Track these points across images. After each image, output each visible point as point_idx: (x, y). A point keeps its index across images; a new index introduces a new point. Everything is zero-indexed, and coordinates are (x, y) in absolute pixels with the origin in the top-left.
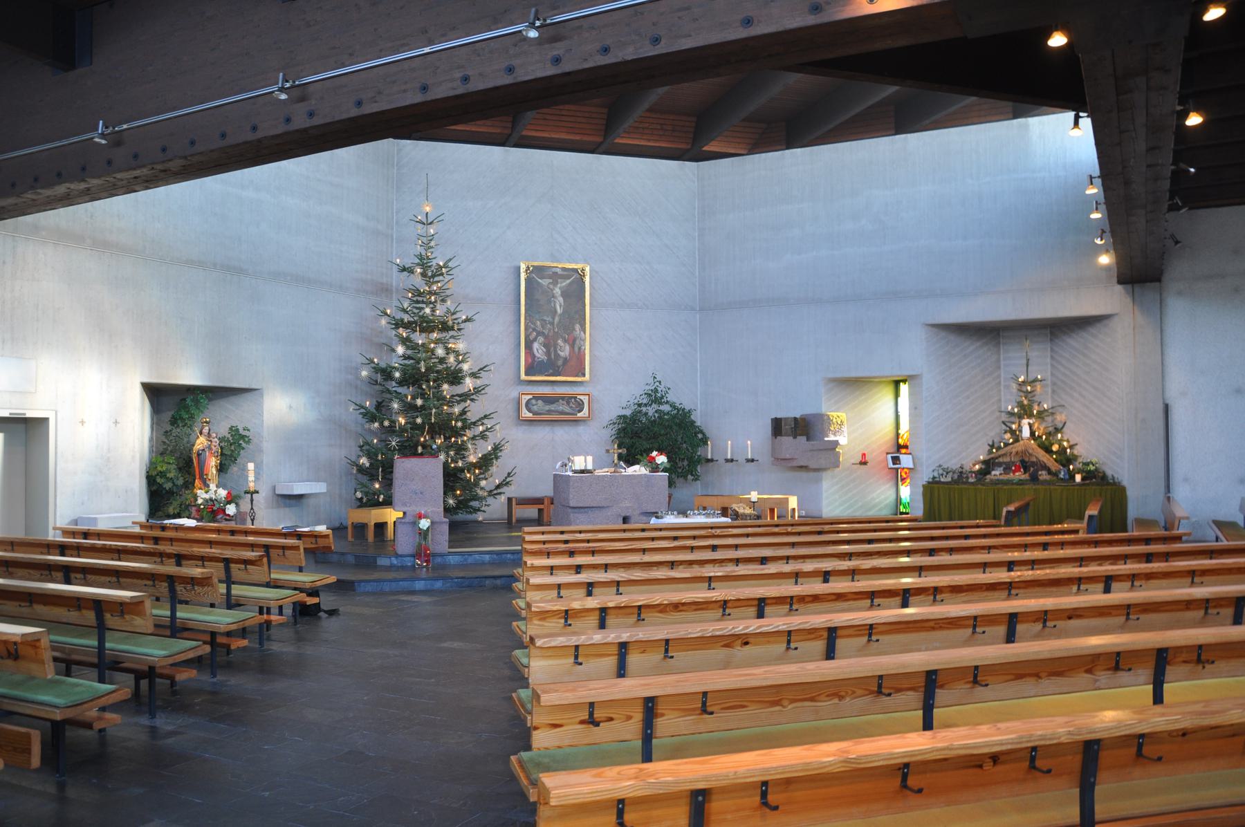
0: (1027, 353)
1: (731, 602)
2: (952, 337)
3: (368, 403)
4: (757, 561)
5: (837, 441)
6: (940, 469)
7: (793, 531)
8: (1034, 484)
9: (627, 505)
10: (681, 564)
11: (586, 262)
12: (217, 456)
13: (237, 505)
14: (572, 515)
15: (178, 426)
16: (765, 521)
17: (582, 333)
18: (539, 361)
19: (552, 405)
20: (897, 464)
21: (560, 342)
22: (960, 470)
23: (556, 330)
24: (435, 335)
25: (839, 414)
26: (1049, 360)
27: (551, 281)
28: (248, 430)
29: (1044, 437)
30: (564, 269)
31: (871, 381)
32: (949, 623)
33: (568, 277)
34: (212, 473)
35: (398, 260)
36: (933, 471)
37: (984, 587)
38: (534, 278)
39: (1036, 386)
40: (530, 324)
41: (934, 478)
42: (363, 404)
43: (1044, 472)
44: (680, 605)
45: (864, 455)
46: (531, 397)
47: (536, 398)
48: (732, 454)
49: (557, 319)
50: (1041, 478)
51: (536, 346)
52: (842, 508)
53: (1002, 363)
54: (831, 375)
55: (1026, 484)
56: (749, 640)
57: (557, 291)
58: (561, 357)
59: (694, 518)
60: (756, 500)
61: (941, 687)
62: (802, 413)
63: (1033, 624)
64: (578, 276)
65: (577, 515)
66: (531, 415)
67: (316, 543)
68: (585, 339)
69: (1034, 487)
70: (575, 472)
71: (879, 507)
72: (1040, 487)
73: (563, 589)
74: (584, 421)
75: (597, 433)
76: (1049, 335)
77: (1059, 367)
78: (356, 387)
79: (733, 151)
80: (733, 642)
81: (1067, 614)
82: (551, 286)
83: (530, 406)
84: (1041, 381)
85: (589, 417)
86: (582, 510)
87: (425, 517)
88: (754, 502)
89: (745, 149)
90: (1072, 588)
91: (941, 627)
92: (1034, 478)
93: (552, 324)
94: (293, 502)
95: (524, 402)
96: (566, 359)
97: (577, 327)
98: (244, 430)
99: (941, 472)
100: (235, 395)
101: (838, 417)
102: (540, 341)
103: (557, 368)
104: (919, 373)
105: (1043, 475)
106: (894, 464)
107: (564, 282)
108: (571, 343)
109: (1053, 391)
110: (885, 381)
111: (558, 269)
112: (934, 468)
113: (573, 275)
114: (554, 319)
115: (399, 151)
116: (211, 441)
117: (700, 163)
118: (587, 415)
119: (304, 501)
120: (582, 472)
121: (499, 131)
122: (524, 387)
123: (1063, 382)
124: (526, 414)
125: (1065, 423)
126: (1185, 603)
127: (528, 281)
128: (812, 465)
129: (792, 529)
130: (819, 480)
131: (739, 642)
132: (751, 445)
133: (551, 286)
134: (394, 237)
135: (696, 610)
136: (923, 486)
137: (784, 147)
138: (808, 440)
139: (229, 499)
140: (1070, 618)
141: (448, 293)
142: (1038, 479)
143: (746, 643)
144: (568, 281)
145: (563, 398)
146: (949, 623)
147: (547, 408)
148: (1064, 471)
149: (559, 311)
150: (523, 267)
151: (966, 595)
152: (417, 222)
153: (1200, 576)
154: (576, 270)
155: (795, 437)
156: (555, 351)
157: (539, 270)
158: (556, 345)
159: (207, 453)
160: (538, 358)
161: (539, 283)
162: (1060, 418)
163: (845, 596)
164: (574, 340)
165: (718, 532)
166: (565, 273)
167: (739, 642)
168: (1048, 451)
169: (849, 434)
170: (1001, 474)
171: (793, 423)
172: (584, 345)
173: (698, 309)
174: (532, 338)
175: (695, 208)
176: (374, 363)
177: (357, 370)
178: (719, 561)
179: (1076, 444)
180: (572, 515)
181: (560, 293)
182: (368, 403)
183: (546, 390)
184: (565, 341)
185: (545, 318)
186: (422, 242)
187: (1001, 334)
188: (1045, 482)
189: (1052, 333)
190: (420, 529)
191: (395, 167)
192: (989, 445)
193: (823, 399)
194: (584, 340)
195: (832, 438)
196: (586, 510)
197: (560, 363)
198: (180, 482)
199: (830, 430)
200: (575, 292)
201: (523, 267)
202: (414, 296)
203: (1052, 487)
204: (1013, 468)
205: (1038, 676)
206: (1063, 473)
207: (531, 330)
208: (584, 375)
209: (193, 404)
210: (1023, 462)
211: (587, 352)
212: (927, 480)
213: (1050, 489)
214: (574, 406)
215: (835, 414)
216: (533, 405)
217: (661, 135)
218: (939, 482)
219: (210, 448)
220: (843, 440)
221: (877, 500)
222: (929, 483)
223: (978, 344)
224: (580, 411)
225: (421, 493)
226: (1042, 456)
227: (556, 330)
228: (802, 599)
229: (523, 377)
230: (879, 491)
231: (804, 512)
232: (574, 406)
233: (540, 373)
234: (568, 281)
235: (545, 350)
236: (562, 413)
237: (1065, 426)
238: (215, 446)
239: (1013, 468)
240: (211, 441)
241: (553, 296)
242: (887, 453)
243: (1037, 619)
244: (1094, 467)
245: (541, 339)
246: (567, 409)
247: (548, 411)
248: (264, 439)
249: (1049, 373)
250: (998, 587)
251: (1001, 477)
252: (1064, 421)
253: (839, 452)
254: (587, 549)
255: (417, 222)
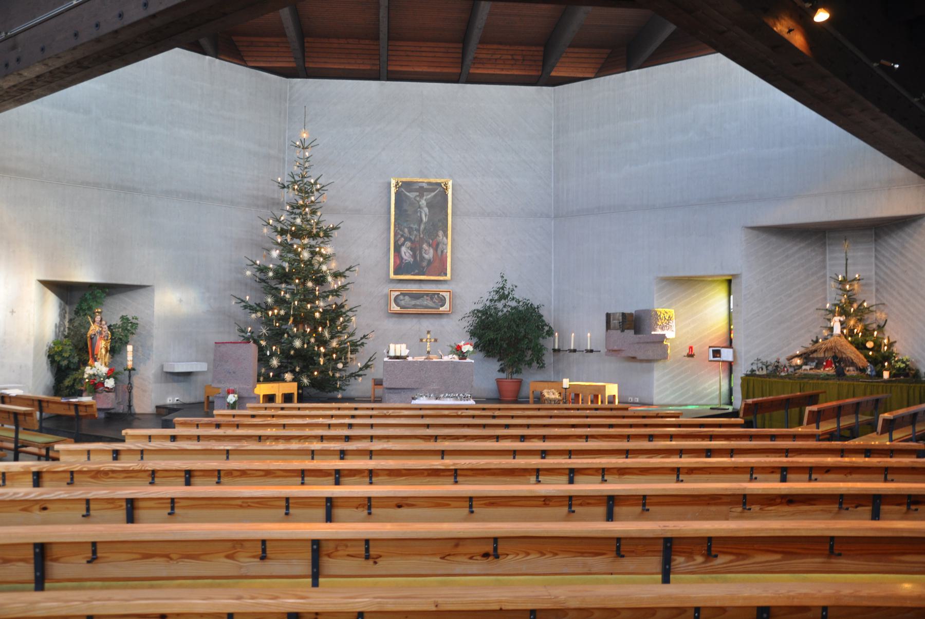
0: (846, 253)
1: (160, 472)
2: (773, 239)
3: (248, 297)
4: (341, 439)
5: (664, 335)
6: (759, 362)
7: (463, 414)
8: (839, 380)
9: (435, 387)
10: (268, 439)
11: (451, 177)
12: (107, 340)
13: (116, 379)
14: (387, 395)
15: (80, 315)
16: (577, 405)
17: (445, 238)
18: (406, 263)
19: (418, 301)
20: (717, 357)
21: (425, 246)
22: (776, 364)
23: (422, 236)
24: (306, 241)
25: (667, 310)
26: (873, 259)
27: (418, 194)
28: (136, 319)
29: (860, 334)
30: (429, 184)
31: (704, 281)
32: (258, 503)
33: (433, 190)
34: (101, 354)
35: (279, 179)
36: (752, 364)
37: (426, 473)
38: (402, 191)
39: (853, 285)
40: (398, 231)
41: (753, 371)
42: (244, 299)
43: (851, 368)
44: (110, 473)
45: (691, 348)
46: (398, 293)
47: (404, 294)
48: (559, 346)
49: (422, 227)
50: (848, 374)
51: (403, 249)
52: (672, 397)
53: (828, 262)
54: (662, 275)
55: (831, 379)
56: (47, 505)
57: (423, 202)
58: (425, 259)
59: (444, 400)
60: (568, 387)
61: (56, 560)
62: (637, 309)
63: (355, 510)
64: (442, 189)
65: (391, 395)
66: (398, 308)
67: (86, 412)
68: (447, 244)
69: (838, 383)
70: (391, 358)
71: (711, 397)
72: (844, 382)
73: (232, 454)
74: (448, 314)
75: (458, 325)
76: (874, 236)
77: (881, 266)
78: (246, 285)
79: (581, 75)
80: (31, 506)
81: (396, 503)
82: (418, 199)
83: (399, 301)
84: (859, 280)
85: (450, 311)
86: (397, 391)
87: (233, 392)
88: (566, 389)
89: (592, 72)
90: (529, 479)
91: (249, 506)
92: (840, 374)
93: (418, 230)
94: (181, 378)
95: (393, 298)
96: (429, 261)
97: (441, 233)
98: (133, 318)
99: (760, 365)
100: (132, 290)
101: (666, 312)
102: (408, 245)
103: (422, 269)
104: (739, 273)
105: (851, 371)
106: (714, 357)
107: (430, 194)
108: (434, 246)
109: (877, 290)
110: (718, 281)
111: (424, 184)
112: (752, 361)
113: (438, 188)
114: (420, 226)
115: (291, 88)
116: (101, 327)
117: (556, 88)
118: (448, 309)
119: (193, 378)
120: (397, 358)
121: (369, 67)
122: (394, 285)
123: (886, 282)
124: (395, 308)
125: (886, 321)
126: (543, 499)
127: (397, 194)
128: (640, 356)
129: (462, 413)
130: (651, 371)
131: (37, 507)
132: (590, 337)
133: (418, 199)
134: (286, 159)
135: (126, 477)
136: (742, 378)
137: (625, 69)
138: (635, 333)
139: (109, 375)
140: (399, 506)
141: (318, 206)
142: (845, 375)
143: (45, 509)
144: (433, 194)
145: (427, 295)
146: (258, 503)
147: (413, 302)
148: (871, 368)
149: (424, 219)
150: (393, 182)
151: (405, 480)
152: (296, 147)
153: (687, 473)
154: (439, 184)
155: (623, 331)
156: (421, 253)
157: (408, 185)
158: (421, 249)
159: (98, 337)
160: (406, 260)
161: (405, 195)
162: (880, 316)
163: (274, 473)
164: (438, 245)
165: (460, 413)
166: (430, 187)
167: (37, 507)
168: (861, 346)
169: (677, 330)
170: (811, 369)
171: (621, 318)
172: (446, 249)
173: (553, 217)
174: (400, 242)
175: (551, 128)
176: (256, 264)
177: (241, 271)
178: (304, 437)
179: (895, 342)
180: (387, 395)
181: (425, 204)
182: (248, 297)
183: (414, 288)
184: (429, 245)
185: (412, 226)
186: (299, 164)
187: (827, 235)
188: (853, 378)
189: (876, 234)
190: (229, 403)
191: (288, 102)
192: (812, 341)
193: (655, 296)
194: (446, 245)
195: (659, 332)
196: (400, 391)
197: (425, 264)
198: (76, 360)
199: (657, 325)
200: (439, 204)
201: (393, 182)
202: (293, 207)
203: (855, 383)
204: (825, 363)
205: (168, 557)
206: (869, 370)
207: (399, 236)
208: (446, 275)
209: (91, 297)
210: (835, 357)
211: (449, 254)
212: (745, 373)
213: (853, 384)
214: (437, 301)
215: (663, 310)
216: (401, 300)
217: (512, 65)
218: (755, 375)
219: (101, 333)
220: (670, 334)
221: (709, 390)
222: (747, 375)
223: (802, 245)
224: (442, 306)
225: (234, 373)
226: (851, 352)
227: (422, 236)
228: (230, 473)
229: (392, 276)
230: (711, 382)
231: (638, 399)
232: (437, 301)
233: (408, 273)
234: (433, 194)
235: (411, 253)
236: (427, 307)
237: (886, 325)
238: (105, 332)
239: (825, 363)
240: (101, 327)
241: (420, 207)
242: (710, 347)
243: (360, 505)
244: (904, 365)
245: (408, 244)
246: (430, 304)
247: (413, 305)
248: (154, 327)
249: (873, 273)
250: (442, 474)
251: (812, 372)
252: (885, 320)
253: (667, 345)
254: (228, 423)
255: (296, 147)
